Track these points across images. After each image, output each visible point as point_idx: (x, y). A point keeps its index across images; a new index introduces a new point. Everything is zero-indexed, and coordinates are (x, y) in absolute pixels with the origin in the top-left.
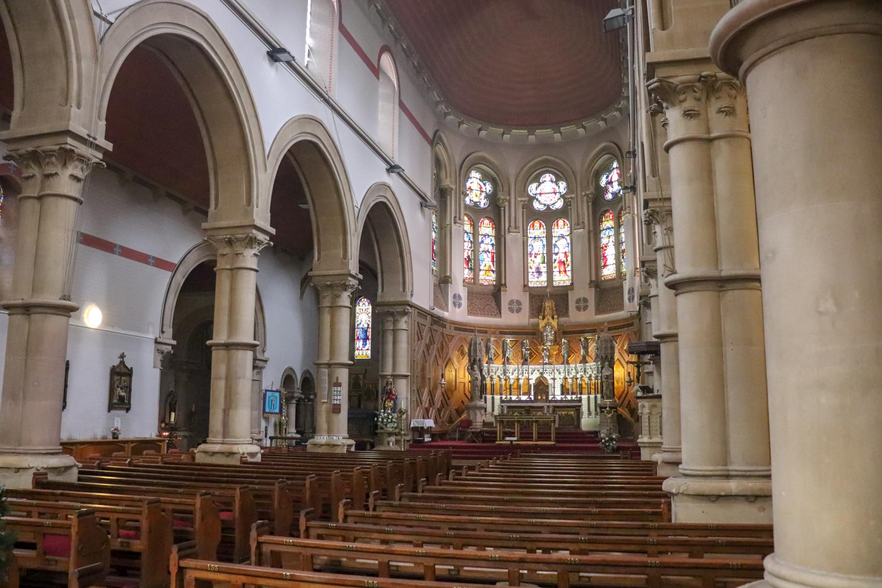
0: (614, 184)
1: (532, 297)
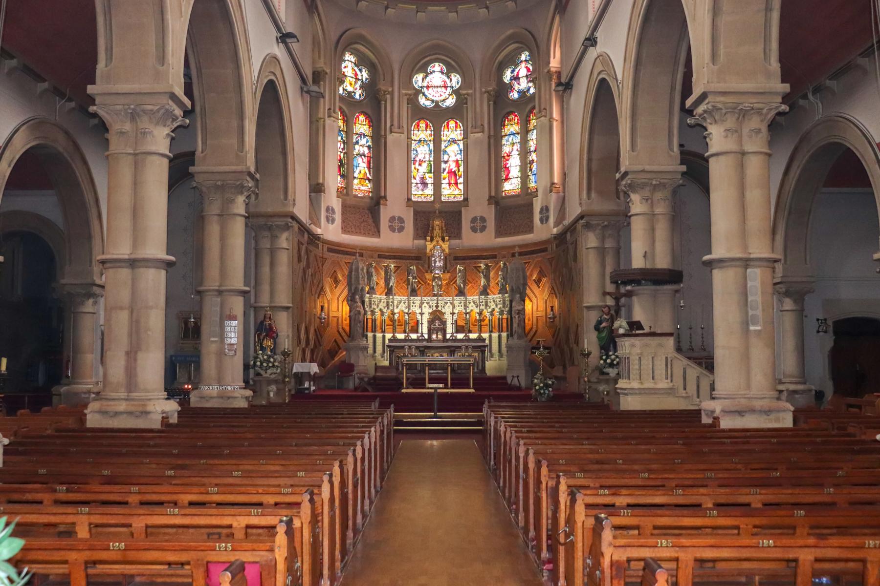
0: (521, 80)
1: (416, 213)
